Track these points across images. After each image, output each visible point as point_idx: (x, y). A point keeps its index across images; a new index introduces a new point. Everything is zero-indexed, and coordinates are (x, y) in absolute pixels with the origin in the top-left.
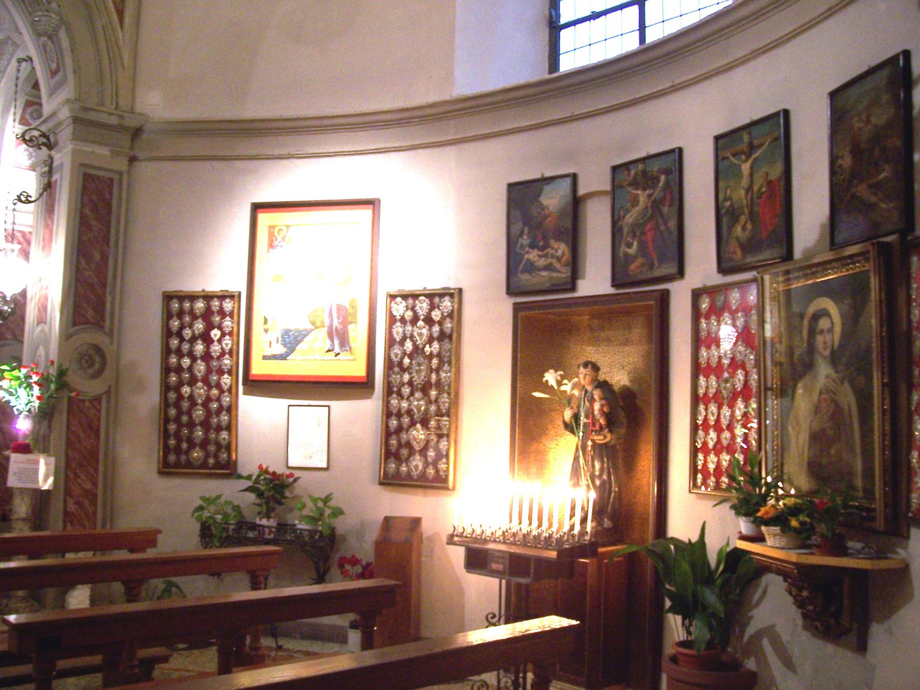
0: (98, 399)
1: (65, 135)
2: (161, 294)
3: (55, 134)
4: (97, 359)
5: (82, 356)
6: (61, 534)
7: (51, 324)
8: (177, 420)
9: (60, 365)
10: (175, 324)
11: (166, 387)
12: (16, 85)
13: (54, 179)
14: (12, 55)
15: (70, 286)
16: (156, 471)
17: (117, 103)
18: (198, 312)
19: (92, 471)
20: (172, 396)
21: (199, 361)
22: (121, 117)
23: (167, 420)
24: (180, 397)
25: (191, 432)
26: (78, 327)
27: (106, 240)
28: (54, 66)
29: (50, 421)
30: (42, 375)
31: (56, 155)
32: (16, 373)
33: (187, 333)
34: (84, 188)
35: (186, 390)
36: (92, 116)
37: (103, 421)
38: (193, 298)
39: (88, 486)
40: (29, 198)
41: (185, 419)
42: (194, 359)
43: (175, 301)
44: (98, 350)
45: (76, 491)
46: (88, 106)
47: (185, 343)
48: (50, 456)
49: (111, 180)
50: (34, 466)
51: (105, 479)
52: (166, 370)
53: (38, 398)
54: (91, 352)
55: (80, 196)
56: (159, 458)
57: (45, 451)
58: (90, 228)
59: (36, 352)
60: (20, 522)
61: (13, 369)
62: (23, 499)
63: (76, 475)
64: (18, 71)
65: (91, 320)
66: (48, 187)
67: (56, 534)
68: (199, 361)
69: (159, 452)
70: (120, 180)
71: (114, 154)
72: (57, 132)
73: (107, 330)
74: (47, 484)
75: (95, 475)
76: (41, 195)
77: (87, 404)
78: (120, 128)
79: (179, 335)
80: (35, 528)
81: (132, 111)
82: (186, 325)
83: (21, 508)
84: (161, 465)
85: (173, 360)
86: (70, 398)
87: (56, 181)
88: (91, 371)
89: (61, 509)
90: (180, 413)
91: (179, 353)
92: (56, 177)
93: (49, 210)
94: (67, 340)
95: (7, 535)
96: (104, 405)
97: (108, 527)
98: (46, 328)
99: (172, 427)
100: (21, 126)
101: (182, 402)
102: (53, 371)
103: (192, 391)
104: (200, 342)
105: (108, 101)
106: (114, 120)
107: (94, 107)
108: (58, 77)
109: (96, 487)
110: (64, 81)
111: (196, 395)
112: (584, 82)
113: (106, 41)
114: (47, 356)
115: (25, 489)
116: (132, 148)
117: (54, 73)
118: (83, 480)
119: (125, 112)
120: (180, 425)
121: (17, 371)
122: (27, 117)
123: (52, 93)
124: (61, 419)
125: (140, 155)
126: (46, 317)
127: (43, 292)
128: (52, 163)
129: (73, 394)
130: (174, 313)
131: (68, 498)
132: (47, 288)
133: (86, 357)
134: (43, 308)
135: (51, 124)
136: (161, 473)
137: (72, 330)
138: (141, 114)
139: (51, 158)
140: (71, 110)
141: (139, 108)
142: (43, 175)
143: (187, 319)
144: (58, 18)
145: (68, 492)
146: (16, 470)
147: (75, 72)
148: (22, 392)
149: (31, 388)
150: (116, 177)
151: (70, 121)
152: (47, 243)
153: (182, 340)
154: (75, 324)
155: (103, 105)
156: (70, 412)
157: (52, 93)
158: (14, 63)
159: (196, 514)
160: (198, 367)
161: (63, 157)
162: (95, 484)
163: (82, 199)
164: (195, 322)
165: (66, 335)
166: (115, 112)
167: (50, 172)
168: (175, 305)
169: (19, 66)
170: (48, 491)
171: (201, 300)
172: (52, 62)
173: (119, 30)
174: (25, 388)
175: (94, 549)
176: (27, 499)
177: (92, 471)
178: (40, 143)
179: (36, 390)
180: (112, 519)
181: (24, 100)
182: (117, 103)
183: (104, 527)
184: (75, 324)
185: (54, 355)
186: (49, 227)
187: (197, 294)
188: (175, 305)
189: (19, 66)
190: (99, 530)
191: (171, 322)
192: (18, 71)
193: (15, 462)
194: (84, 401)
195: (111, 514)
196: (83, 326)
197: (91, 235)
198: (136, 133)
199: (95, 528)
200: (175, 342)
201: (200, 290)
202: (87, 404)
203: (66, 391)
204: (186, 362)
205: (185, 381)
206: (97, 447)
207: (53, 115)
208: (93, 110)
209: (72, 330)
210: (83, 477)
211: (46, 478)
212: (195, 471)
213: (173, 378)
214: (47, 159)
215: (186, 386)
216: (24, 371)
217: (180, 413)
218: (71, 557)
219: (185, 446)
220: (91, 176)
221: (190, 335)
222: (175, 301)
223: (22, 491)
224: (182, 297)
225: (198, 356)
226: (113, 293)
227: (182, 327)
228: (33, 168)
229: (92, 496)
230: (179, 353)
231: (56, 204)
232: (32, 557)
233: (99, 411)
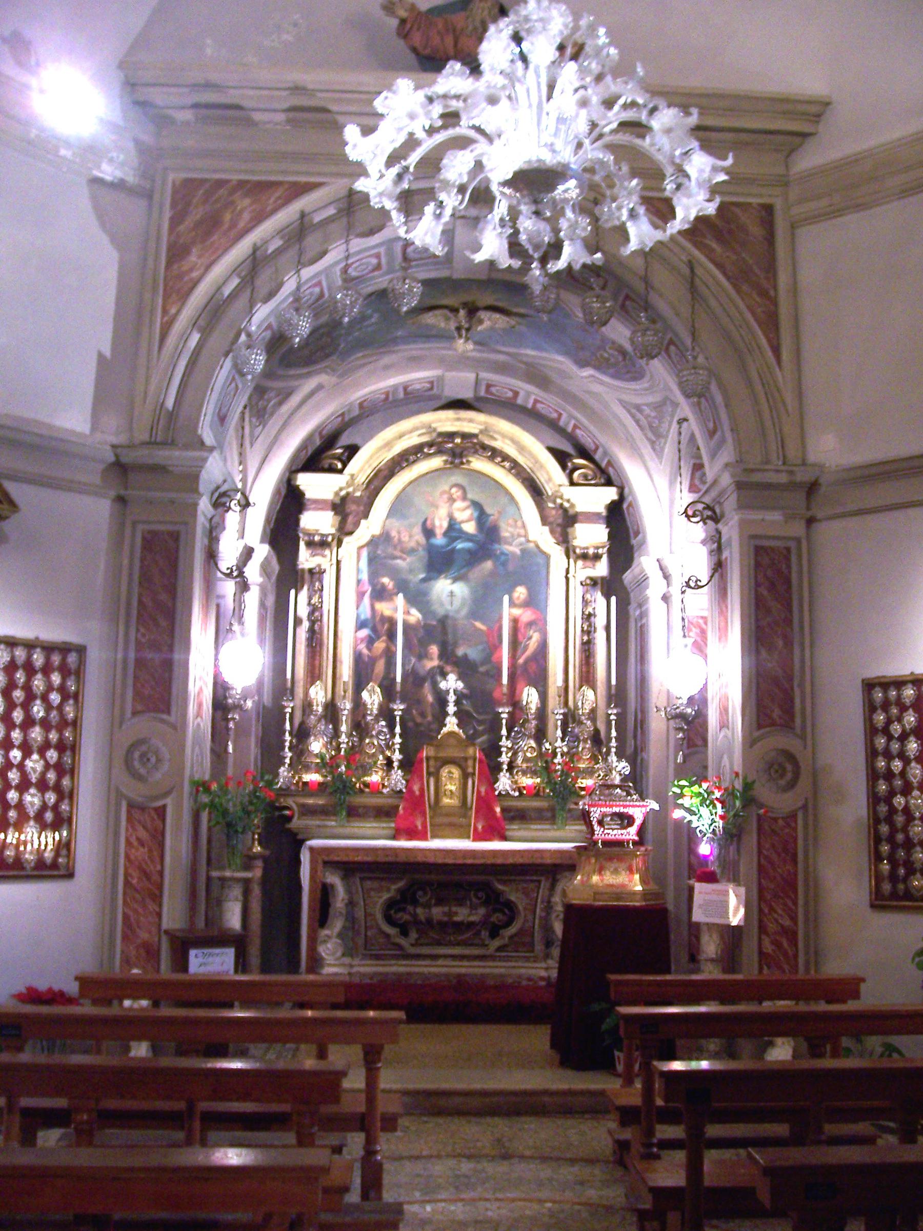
0: (793, 816)
1: (730, 504)
2: (859, 684)
3: (720, 504)
4: (789, 767)
5: (770, 765)
6: (756, 978)
7: (733, 729)
8: (891, 839)
9: (745, 778)
10: (880, 718)
11: (874, 799)
12: (679, 451)
13: (724, 557)
14: (672, 416)
15: (750, 681)
16: (868, 903)
17: (784, 456)
18: (908, 702)
19: (790, 904)
20: (883, 809)
21: (913, 764)
22: (791, 473)
23: (878, 840)
24: (893, 810)
25: (909, 853)
26: (762, 731)
27: (789, 621)
28: (711, 425)
29: (739, 841)
30: (726, 790)
31: (724, 530)
32: (696, 789)
33: (896, 729)
34: (758, 565)
35: (899, 801)
36: (757, 478)
37: (800, 843)
38: (899, 683)
39: (787, 923)
40: (699, 583)
41: (900, 837)
42: (906, 761)
43: (877, 689)
44: (791, 757)
45: (772, 927)
46: (751, 466)
47: (894, 741)
48: (739, 885)
49: (788, 549)
50: (722, 898)
51: (806, 913)
52: (873, 776)
53: (721, 817)
54: (781, 759)
55: (752, 572)
56: (871, 889)
57: (735, 879)
58: (768, 611)
59: (720, 762)
60: (709, 964)
61: (692, 784)
62: (711, 936)
63: (772, 909)
64: (680, 433)
65: (778, 721)
66: (718, 567)
67: (750, 978)
68: (913, 764)
69: (870, 881)
70: (799, 549)
71: (789, 518)
72: (722, 500)
73: (798, 731)
74: (736, 917)
75: (794, 908)
76: (712, 577)
77: (781, 822)
78: (792, 486)
79: (886, 731)
80: (725, 971)
81: (804, 464)
82: (894, 719)
83: (710, 947)
84: (873, 897)
85: (881, 763)
86: (759, 817)
87: (726, 559)
88: (782, 782)
89: (756, 949)
90: (894, 830)
91: (888, 755)
92: (725, 554)
93: (722, 592)
94: (751, 746)
95: (694, 977)
96: (800, 822)
97: (812, 972)
98: (729, 733)
99: (885, 848)
100: (691, 495)
101: (895, 817)
102: (738, 785)
103: (907, 802)
104: (912, 738)
105: (774, 457)
106: (783, 478)
107: (758, 467)
108: (717, 436)
109: (796, 923)
110: (723, 441)
111: (912, 807)
112: (810, 601)
113: (763, 385)
114: (731, 768)
115: (714, 924)
116: (808, 508)
117: (712, 434)
118: (781, 916)
119: (795, 465)
120: (894, 846)
121: (697, 786)
122: (697, 482)
123: (713, 455)
124: (751, 840)
125: (819, 515)
126: (728, 720)
127: (723, 691)
128: (720, 537)
129: (762, 811)
130: (878, 705)
131: (763, 937)
132: (727, 686)
133: (776, 767)
134: (724, 711)
135: (713, 494)
136: (873, 906)
137: (757, 734)
138: (814, 465)
139: (719, 533)
140: (732, 476)
141: (812, 458)
142: (711, 552)
143: (895, 711)
144: (706, 373)
145: (762, 929)
146: (701, 902)
147: (732, 430)
148: (704, 811)
149: (715, 807)
150: (792, 545)
151: (733, 487)
152: (723, 632)
153: (890, 738)
154: (760, 726)
155: (768, 462)
156: (760, 830)
157: (713, 455)
158: (675, 426)
159: (917, 959)
160: (913, 771)
161: (730, 530)
162: (794, 919)
163: (756, 577)
164: (905, 714)
165: (750, 742)
166: (783, 468)
167: (719, 549)
168: (879, 695)
169: (680, 428)
170: (737, 927)
171: (910, 686)
172: (709, 420)
173: (777, 370)
174: (707, 806)
175: (796, 998)
176: (715, 936)
177: (790, 904)
178: (705, 516)
179: (720, 810)
180: (817, 963)
181: (691, 464)
182: (784, 456)
183: (807, 969)
184: (760, 726)
185: (738, 766)
186: (723, 613)
187: (904, 679)
188: (879, 695)
189: (680, 428)
190: (801, 974)
191: (875, 716)
192: (680, 433)
193: (700, 893)
194: (775, 820)
195: (816, 956)
196: (768, 729)
197: (769, 619)
198: (812, 488)
199: (797, 972)
200: (881, 741)
201: (907, 672)
202: (781, 822)
203: (754, 808)
204: (897, 765)
205: (898, 790)
206: (796, 874)
207: (715, 482)
208: (759, 470)
209: (757, 734)
210: (780, 912)
211: (736, 910)
212: (916, 904)
213: (883, 787)
214: (714, 533)
215: (899, 796)
216: (705, 785)
217: (894, 830)
218: (767, 1006)
219: (902, 871)
220: (762, 547)
221: (900, 731)
222: (877, 689)
223: (710, 926)
224: (886, 684)
225: (912, 757)
226: (802, 685)
227: (889, 722)
228: (704, 542)
229: (792, 936)
230: (888, 755)
231: (729, 585)
232: (723, 1002)
233: (795, 829)
